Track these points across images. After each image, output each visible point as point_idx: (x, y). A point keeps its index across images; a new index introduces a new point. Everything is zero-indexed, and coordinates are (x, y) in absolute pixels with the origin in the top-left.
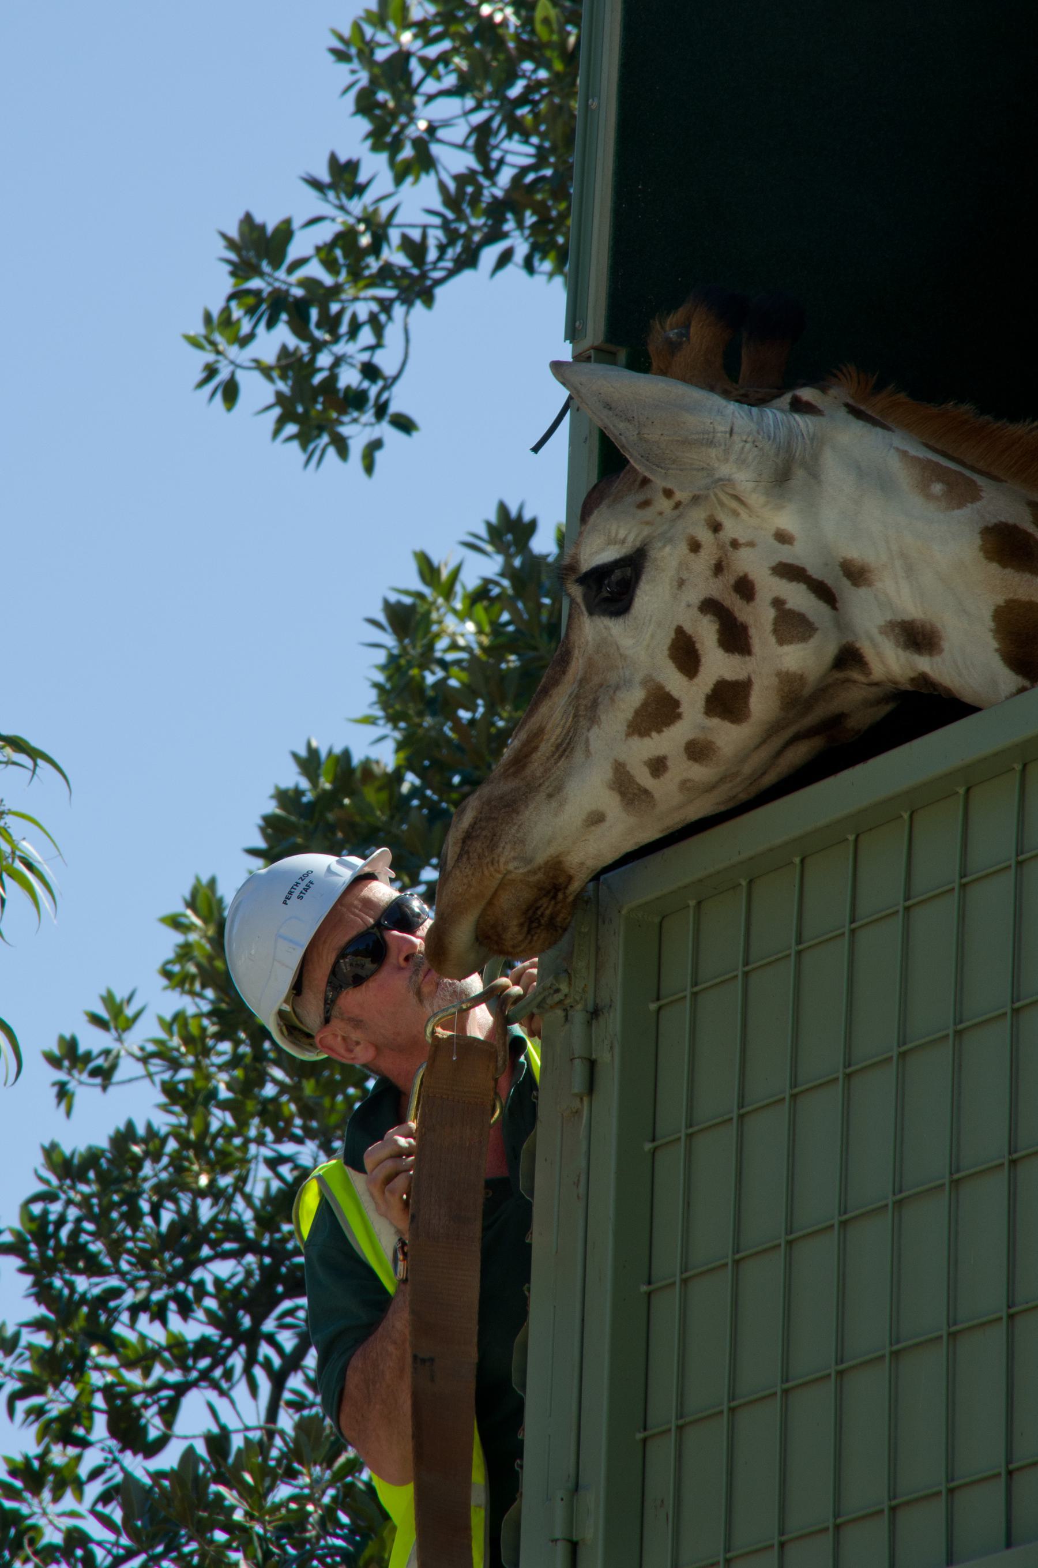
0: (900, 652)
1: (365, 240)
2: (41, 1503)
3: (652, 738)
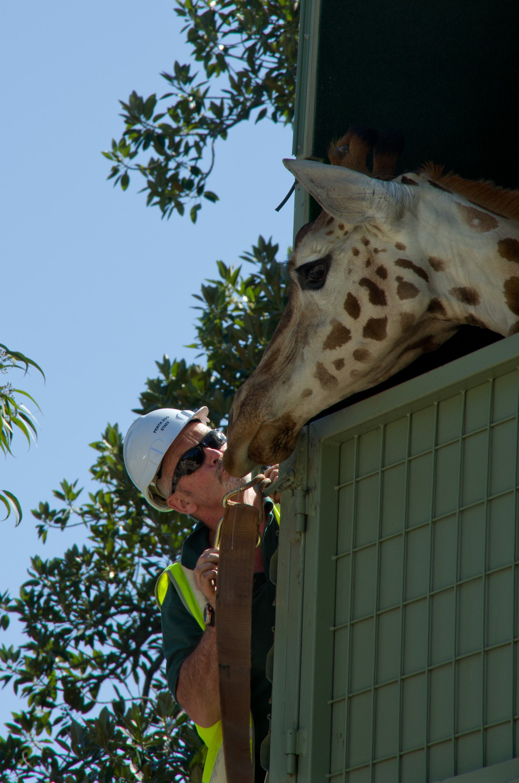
0: (460, 303)
1: (192, 105)
2: (31, 735)
3: (336, 350)
